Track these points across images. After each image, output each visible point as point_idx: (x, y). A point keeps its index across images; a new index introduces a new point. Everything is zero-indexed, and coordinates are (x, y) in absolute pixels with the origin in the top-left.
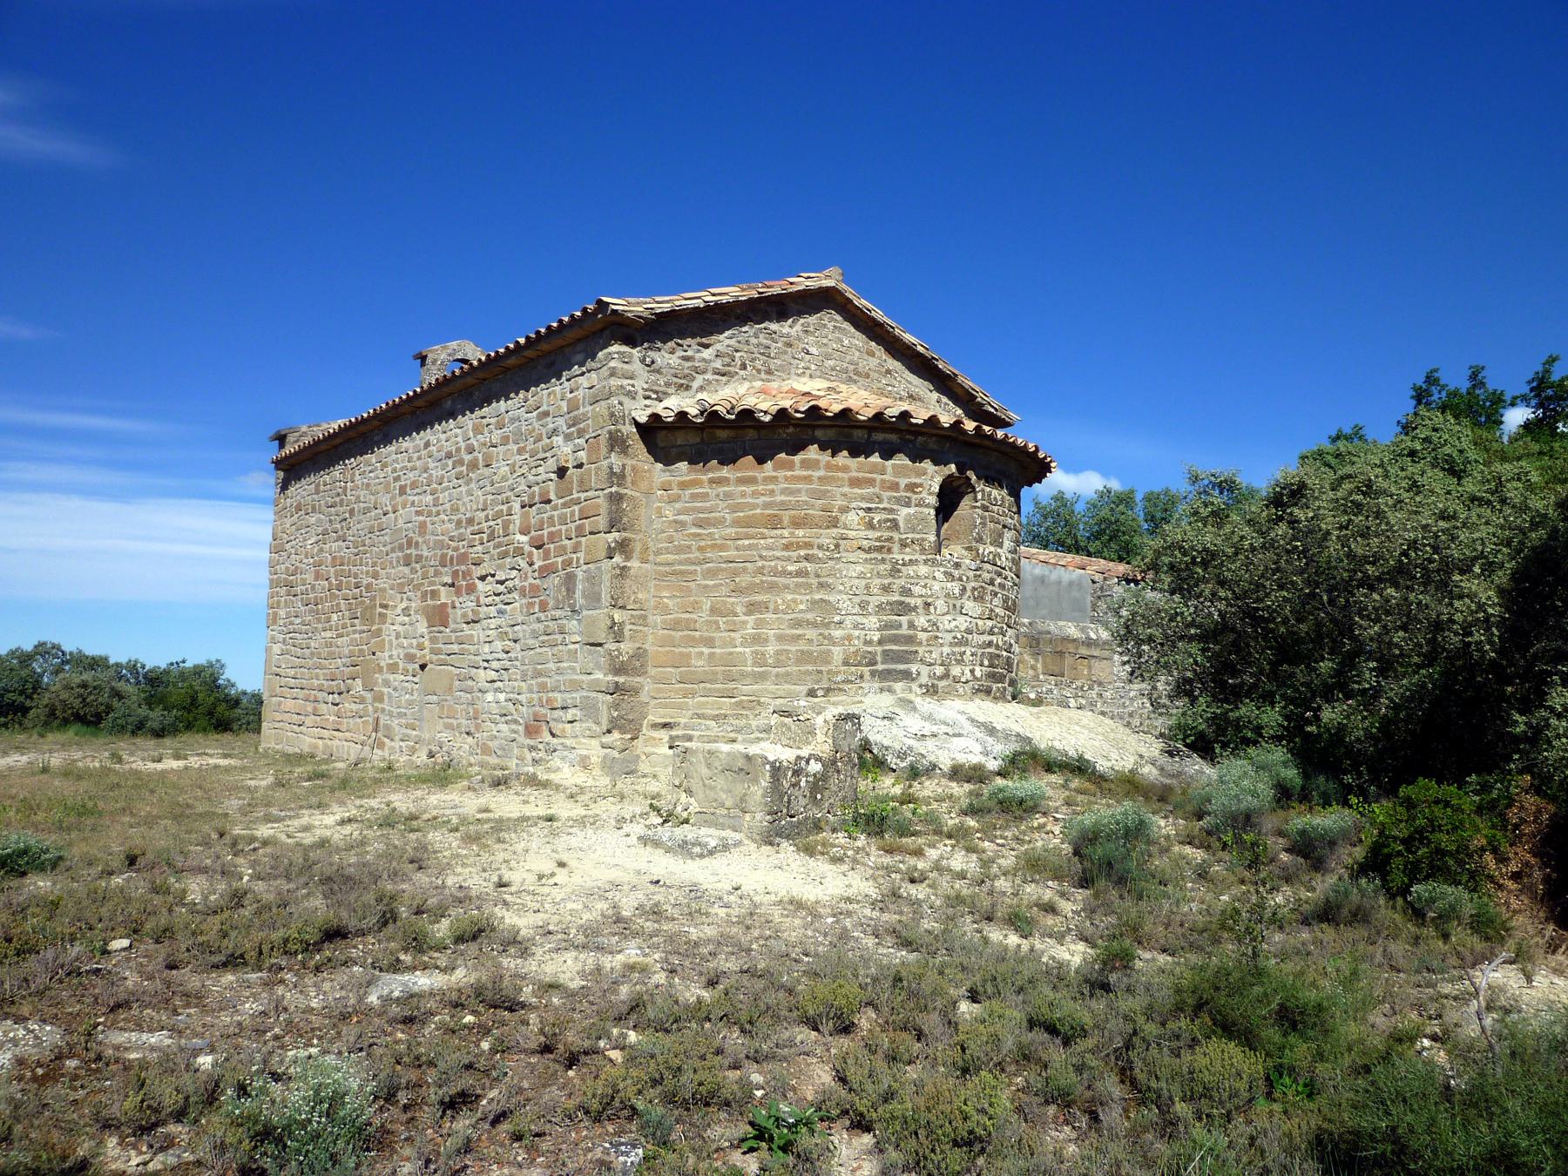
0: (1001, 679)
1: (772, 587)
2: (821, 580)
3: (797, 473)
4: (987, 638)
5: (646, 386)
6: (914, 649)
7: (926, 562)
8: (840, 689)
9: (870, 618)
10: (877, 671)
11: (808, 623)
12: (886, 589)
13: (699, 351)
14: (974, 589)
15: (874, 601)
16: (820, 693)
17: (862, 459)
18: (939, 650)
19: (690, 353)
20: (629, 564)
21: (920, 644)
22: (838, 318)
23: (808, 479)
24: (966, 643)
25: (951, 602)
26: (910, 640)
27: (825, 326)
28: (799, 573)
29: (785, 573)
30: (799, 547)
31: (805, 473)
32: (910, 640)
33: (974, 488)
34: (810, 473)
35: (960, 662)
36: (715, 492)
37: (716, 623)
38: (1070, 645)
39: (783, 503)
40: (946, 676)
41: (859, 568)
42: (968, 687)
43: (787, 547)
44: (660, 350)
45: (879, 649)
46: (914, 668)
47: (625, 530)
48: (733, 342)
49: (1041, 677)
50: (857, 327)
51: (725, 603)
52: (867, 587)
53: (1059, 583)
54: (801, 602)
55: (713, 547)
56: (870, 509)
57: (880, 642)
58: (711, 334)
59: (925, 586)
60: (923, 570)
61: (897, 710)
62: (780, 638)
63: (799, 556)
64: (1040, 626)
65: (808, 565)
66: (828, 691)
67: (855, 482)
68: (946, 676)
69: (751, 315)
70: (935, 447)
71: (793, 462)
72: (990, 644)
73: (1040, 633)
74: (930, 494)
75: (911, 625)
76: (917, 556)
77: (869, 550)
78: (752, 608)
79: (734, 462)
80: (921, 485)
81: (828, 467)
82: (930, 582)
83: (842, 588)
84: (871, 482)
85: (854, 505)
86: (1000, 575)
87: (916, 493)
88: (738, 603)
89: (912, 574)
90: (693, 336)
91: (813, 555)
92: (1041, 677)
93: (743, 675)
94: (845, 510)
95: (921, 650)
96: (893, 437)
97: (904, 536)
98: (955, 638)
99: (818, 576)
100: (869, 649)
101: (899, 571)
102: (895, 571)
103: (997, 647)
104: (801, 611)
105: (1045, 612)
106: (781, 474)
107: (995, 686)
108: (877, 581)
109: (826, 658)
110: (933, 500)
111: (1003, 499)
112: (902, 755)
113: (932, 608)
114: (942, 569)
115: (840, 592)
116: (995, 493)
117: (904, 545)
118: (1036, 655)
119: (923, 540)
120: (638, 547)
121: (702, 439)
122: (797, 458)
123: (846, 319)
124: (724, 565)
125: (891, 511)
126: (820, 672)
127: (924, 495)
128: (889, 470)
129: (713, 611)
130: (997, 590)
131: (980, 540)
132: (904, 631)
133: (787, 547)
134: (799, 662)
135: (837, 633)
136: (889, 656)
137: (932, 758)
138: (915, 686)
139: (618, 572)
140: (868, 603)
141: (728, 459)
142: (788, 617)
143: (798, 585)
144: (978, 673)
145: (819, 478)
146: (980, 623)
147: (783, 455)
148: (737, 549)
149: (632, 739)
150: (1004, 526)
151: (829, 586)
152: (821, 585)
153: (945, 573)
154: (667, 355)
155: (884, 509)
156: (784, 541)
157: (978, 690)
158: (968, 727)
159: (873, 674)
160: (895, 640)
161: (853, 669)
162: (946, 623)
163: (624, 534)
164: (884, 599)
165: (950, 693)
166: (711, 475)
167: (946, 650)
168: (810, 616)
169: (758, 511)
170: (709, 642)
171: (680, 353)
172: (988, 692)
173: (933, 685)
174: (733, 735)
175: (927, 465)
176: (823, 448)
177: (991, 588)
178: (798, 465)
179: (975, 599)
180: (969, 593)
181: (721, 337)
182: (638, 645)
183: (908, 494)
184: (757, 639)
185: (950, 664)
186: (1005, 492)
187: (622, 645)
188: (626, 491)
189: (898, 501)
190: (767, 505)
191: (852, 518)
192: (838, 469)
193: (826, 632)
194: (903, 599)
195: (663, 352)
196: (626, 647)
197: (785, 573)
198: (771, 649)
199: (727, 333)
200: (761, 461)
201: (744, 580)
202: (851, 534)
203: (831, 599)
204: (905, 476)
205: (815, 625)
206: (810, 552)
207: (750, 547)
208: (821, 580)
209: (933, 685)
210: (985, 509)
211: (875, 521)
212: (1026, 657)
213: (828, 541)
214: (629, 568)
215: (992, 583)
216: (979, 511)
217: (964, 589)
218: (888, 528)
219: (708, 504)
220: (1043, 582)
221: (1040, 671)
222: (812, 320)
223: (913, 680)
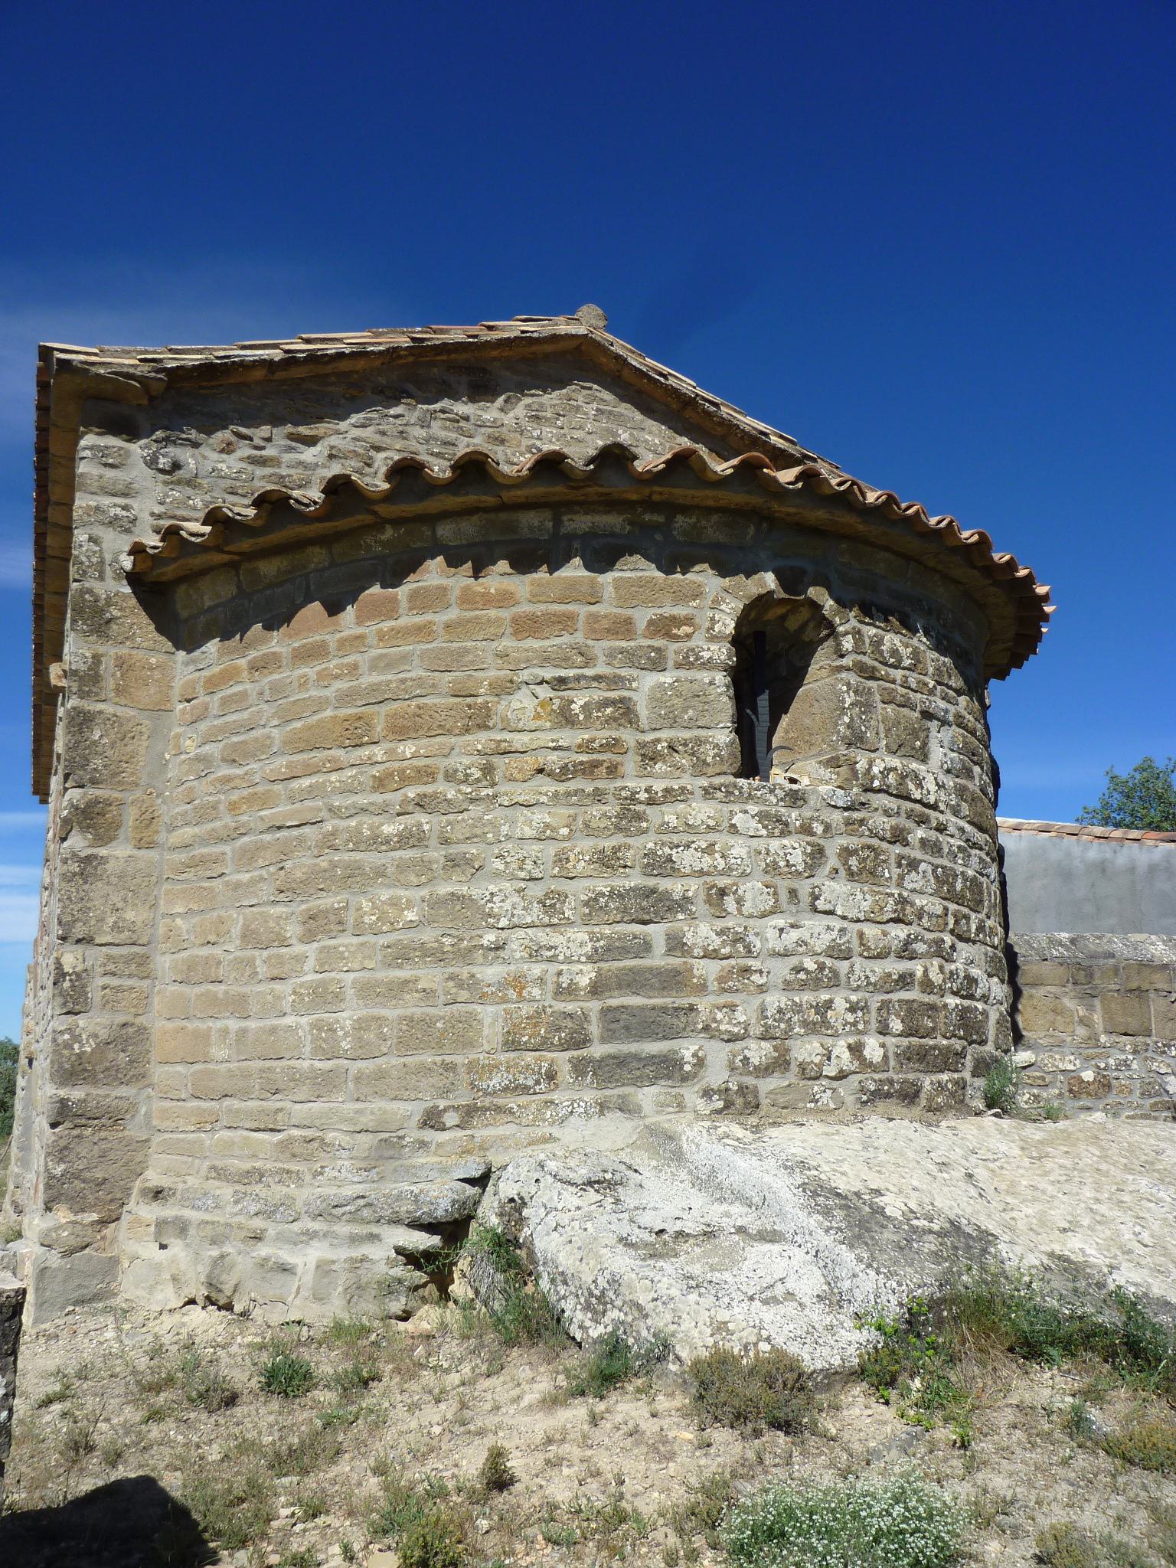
0: (949, 1061)
1: (352, 876)
2: (453, 850)
3: (404, 621)
4: (895, 967)
5: (158, 509)
6: (684, 1002)
7: (708, 793)
8: (499, 1109)
9: (571, 932)
10: (590, 1060)
11: (425, 952)
12: (607, 861)
13: (291, 449)
14: (846, 853)
15: (579, 890)
16: (451, 1119)
17: (542, 575)
18: (756, 1001)
19: (269, 452)
20: (103, 852)
21: (702, 988)
22: (607, 395)
23: (423, 631)
24: (834, 981)
25: (783, 885)
26: (674, 980)
27: (578, 409)
28: (406, 839)
29: (378, 842)
30: (405, 780)
31: (418, 620)
32: (674, 980)
33: (831, 627)
34: (429, 617)
35: (819, 1026)
36: (257, 687)
37: (250, 962)
38: (1157, 976)
39: (374, 688)
40: (780, 1063)
41: (540, 816)
42: (846, 1090)
43: (380, 784)
44: (196, 445)
45: (594, 1006)
46: (687, 1049)
47: (94, 782)
48: (368, 433)
49: (1103, 1038)
50: (648, 411)
51: (265, 917)
52: (561, 859)
53: (1132, 869)
54: (410, 905)
55: (251, 800)
56: (562, 681)
57: (596, 989)
58: (320, 419)
59: (709, 849)
60: (702, 811)
61: (641, 1160)
62: (366, 991)
63: (406, 801)
64: (1092, 944)
65: (424, 818)
66: (469, 1113)
67: (526, 627)
68: (780, 1063)
69: (411, 388)
70: (721, 538)
71: (394, 600)
72: (905, 981)
73: (1093, 956)
74: (713, 639)
75: (676, 945)
76: (687, 781)
77: (564, 773)
78: (316, 925)
79: (288, 619)
80: (688, 621)
81: (467, 599)
82: (722, 839)
83: (499, 865)
84: (566, 622)
85: (524, 675)
86: (922, 821)
87: (676, 638)
88: (287, 917)
89: (672, 820)
90: (276, 421)
91: (434, 796)
92: (1103, 1038)
93: (296, 1078)
94: (505, 688)
95: (703, 1004)
96: (613, 521)
97: (649, 737)
98: (798, 969)
99: (445, 842)
100: (570, 1007)
101: (640, 817)
102: (629, 817)
103: (927, 985)
104: (410, 926)
105: (1113, 921)
106: (371, 629)
107: (927, 1082)
108: (586, 844)
109: (463, 1033)
110: (721, 652)
111: (916, 654)
112: (596, 1303)
113: (730, 903)
114: (753, 809)
115: (497, 875)
116: (892, 640)
117: (649, 756)
118: (1088, 997)
119: (700, 742)
120: (130, 816)
121: (239, 587)
122: (402, 592)
123: (623, 398)
124: (267, 837)
125: (615, 681)
126: (450, 1068)
127: (699, 641)
128: (609, 592)
129: (249, 937)
130: (917, 854)
131: (857, 740)
132: (659, 959)
133: (380, 784)
134: (405, 1044)
135: (490, 973)
136: (616, 1023)
137: (661, 1320)
138: (691, 1095)
139: (75, 867)
140: (563, 897)
141: (277, 618)
142: (382, 940)
143: (403, 867)
144: (873, 1050)
145: (448, 626)
146: (871, 931)
147: (376, 589)
148: (292, 799)
149: (103, 1222)
150: (927, 715)
151: (469, 862)
152: (452, 863)
153: (762, 817)
154: (215, 456)
155: (598, 678)
156: (375, 771)
157: (877, 1095)
158: (796, 1215)
159: (579, 1068)
160: (633, 982)
161: (530, 1057)
162: (769, 934)
163: (93, 792)
164: (602, 886)
165: (788, 1109)
166: (253, 654)
167: (775, 1000)
168: (427, 936)
169: (329, 713)
170: (239, 1006)
171: (244, 450)
172: (909, 1095)
173: (743, 1090)
174: (258, 1223)
175: (704, 577)
176: (454, 561)
177: (897, 849)
178: (404, 604)
179: (852, 876)
180: (833, 861)
181: (343, 425)
182: (121, 1019)
183: (658, 642)
184: (324, 996)
185: (787, 1035)
186: (921, 641)
187: (82, 1021)
188: (100, 706)
189: (631, 658)
190: (345, 698)
191: (523, 704)
192: (488, 600)
193: (464, 972)
194: (651, 882)
195: (203, 450)
196: (92, 1024)
197: (378, 842)
198: (347, 1018)
199: (354, 418)
200: (334, 608)
201: (300, 864)
202: (520, 740)
203: (476, 893)
204: (647, 602)
205: (438, 956)
206: (429, 789)
207: (312, 793)
208: (453, 850)
209: (743, 1090)
210: (867, 673)
211: (576, 707)
212: (1068, 1003)
213: (466, 761)
214: (104, 860)
215: (898, 837)
216: (853, 678)
217: (817, 854)
218: (609, 720)
219: (245, 715)
220: (1104, 871)
221: (1099, 1026)
222: (551, 399)
223: (685, 1078)
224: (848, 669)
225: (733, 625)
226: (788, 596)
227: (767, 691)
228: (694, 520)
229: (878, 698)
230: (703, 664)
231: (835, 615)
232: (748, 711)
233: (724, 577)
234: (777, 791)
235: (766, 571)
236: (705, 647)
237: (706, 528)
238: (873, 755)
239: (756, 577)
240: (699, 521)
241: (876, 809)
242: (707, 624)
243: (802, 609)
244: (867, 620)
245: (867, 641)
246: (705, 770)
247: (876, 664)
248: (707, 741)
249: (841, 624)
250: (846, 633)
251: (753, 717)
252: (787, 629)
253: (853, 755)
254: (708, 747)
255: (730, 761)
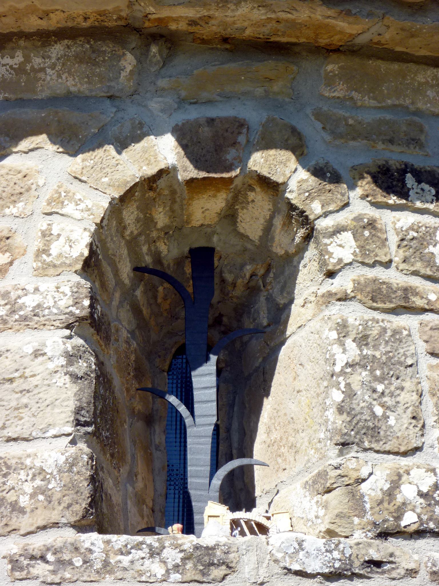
224: (344, 298)
225: (87, 239)
226: (203, 174)
227: (213, 358)
228: (19, 58)
229: (422, 347)
230: (25, 318)
231: (311, 198)
232: (173, 399)
233: (74, 154)
234: (165, 553)
235: (159, 133)
236: (30, 288)
237: (42, 70)
238: (404, 462)
239: (136, 148)
240: (27, 59)
241: (412, 573)
242: (37, 244)
243: (251, 195)
244: (393, 200)
245: (393, 240)
246: (14, 523)
247: (416, 282)
248: (21, 466)
249: (326, 215)
250: (338, 230)
251: (182, 409)
252: (243, 237)
253: (352, 464)
254: (23, 475)
255: (67, 500)
